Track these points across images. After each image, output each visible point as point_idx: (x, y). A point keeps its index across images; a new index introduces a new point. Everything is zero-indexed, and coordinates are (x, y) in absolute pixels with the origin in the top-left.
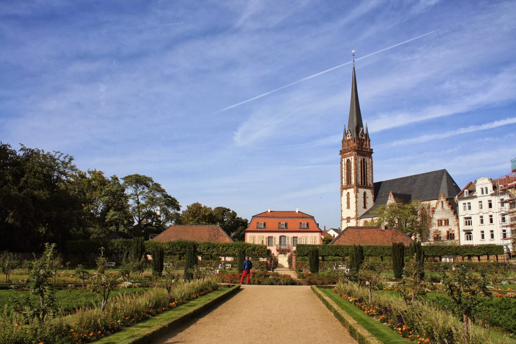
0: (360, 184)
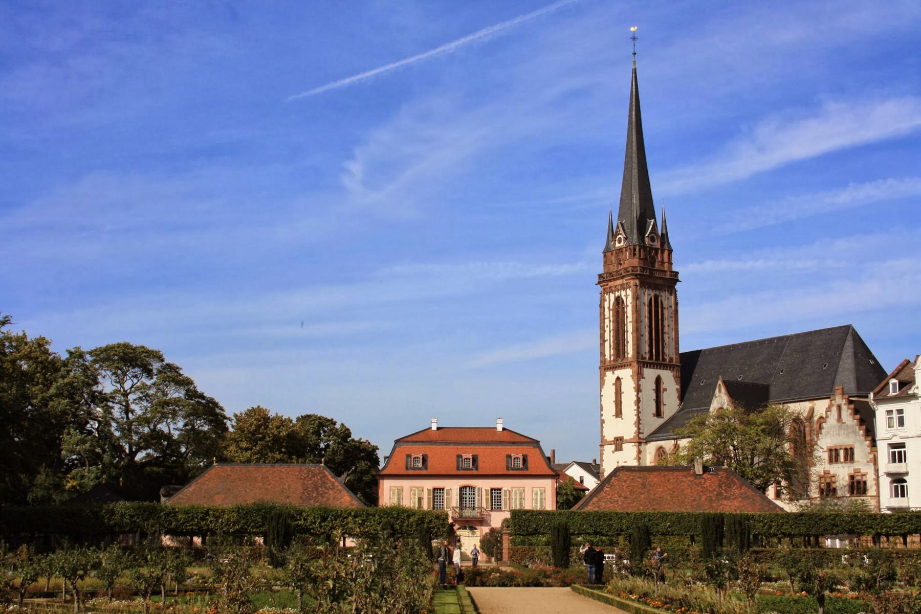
0: (647, 356)
